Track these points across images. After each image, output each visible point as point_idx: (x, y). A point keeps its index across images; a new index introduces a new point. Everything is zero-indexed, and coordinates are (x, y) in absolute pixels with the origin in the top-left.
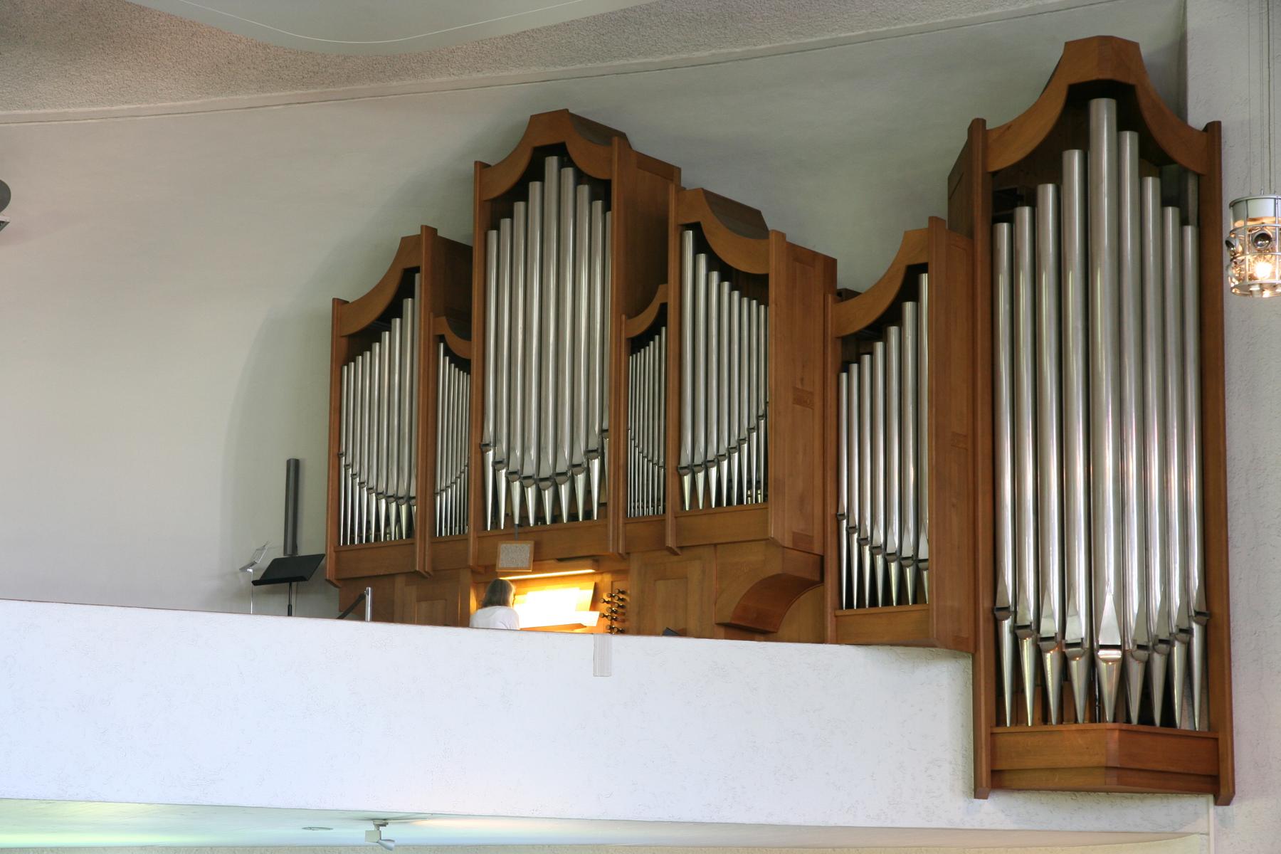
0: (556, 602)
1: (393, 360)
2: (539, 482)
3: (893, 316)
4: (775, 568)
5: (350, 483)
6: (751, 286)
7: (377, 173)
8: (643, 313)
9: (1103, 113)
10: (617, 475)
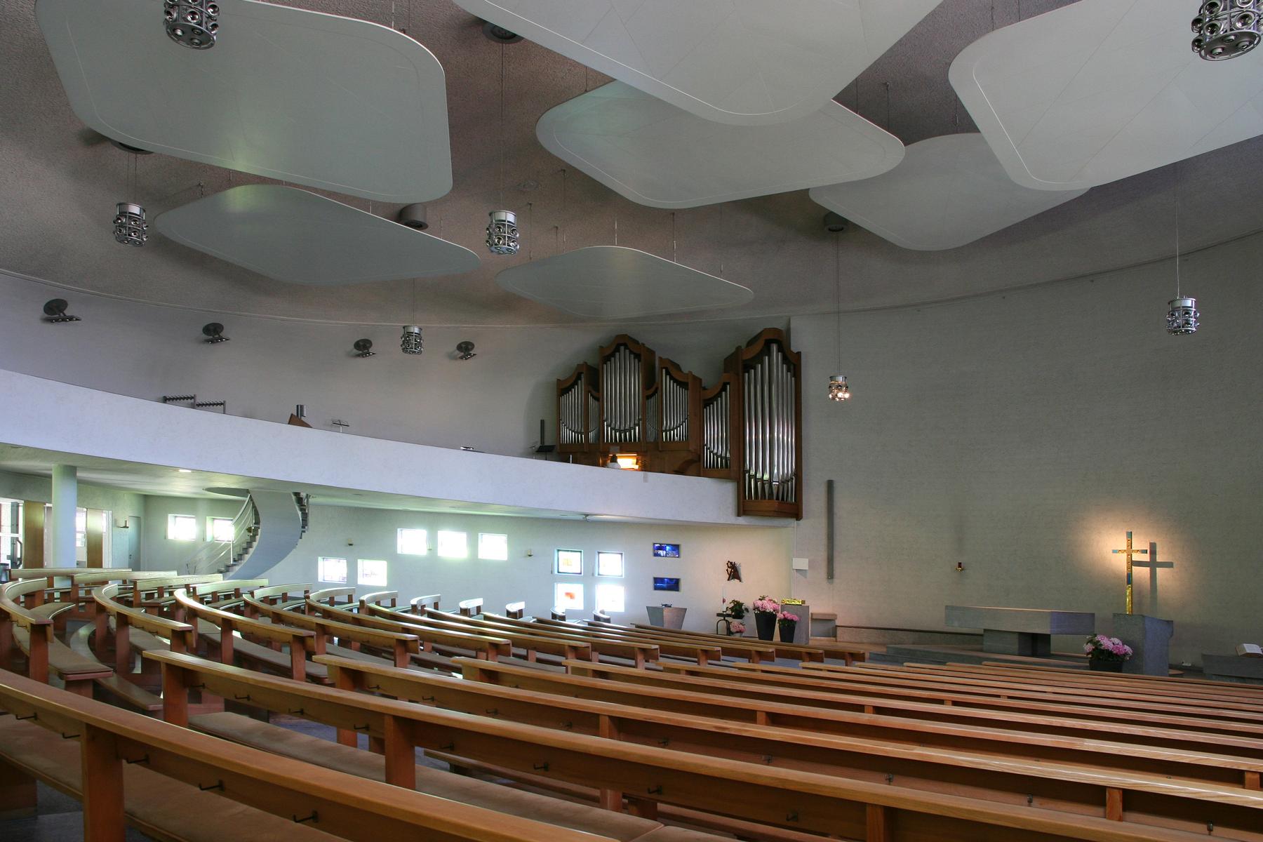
0: (627, 462)
1: (575, 397)
2: (625, 431)
3: (719, 395)
4: (690, 457)
5: (562, 426)
6: (683, 385)
7: (570, 346)
8: (651, 387)
9: (774, 347)
10: (644, 431)
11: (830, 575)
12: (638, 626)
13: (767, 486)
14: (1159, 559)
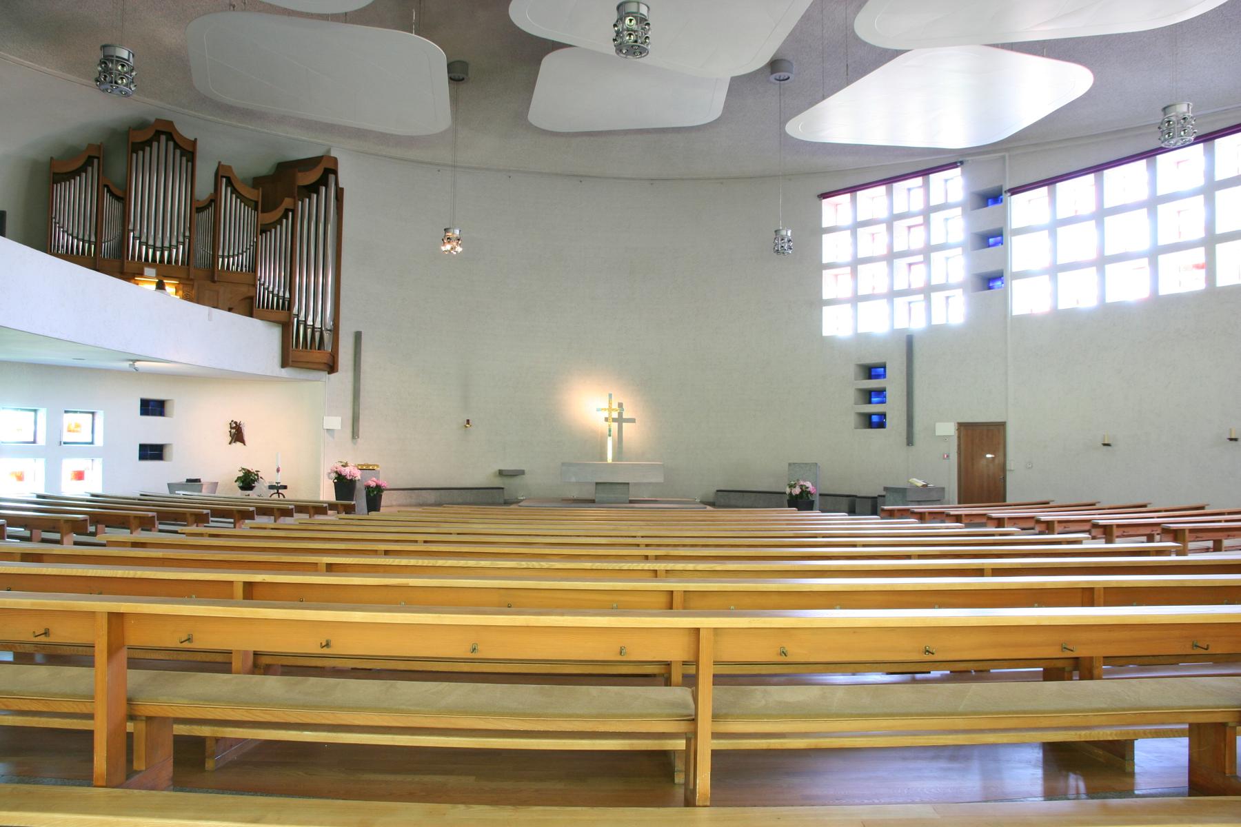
10: (189, 254)
11: (355, 434)
12: (93, 495)
13: (317, 335)
14: (625, 416)
